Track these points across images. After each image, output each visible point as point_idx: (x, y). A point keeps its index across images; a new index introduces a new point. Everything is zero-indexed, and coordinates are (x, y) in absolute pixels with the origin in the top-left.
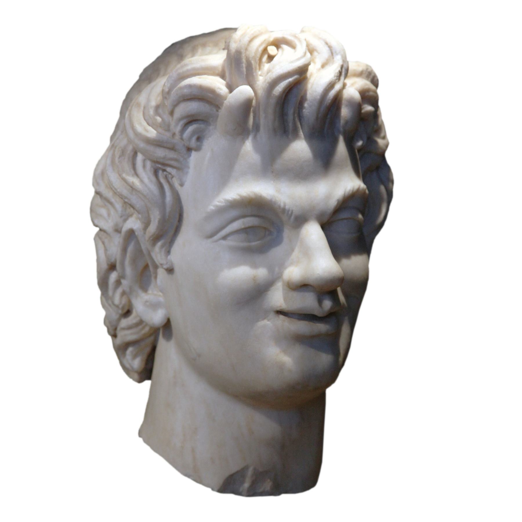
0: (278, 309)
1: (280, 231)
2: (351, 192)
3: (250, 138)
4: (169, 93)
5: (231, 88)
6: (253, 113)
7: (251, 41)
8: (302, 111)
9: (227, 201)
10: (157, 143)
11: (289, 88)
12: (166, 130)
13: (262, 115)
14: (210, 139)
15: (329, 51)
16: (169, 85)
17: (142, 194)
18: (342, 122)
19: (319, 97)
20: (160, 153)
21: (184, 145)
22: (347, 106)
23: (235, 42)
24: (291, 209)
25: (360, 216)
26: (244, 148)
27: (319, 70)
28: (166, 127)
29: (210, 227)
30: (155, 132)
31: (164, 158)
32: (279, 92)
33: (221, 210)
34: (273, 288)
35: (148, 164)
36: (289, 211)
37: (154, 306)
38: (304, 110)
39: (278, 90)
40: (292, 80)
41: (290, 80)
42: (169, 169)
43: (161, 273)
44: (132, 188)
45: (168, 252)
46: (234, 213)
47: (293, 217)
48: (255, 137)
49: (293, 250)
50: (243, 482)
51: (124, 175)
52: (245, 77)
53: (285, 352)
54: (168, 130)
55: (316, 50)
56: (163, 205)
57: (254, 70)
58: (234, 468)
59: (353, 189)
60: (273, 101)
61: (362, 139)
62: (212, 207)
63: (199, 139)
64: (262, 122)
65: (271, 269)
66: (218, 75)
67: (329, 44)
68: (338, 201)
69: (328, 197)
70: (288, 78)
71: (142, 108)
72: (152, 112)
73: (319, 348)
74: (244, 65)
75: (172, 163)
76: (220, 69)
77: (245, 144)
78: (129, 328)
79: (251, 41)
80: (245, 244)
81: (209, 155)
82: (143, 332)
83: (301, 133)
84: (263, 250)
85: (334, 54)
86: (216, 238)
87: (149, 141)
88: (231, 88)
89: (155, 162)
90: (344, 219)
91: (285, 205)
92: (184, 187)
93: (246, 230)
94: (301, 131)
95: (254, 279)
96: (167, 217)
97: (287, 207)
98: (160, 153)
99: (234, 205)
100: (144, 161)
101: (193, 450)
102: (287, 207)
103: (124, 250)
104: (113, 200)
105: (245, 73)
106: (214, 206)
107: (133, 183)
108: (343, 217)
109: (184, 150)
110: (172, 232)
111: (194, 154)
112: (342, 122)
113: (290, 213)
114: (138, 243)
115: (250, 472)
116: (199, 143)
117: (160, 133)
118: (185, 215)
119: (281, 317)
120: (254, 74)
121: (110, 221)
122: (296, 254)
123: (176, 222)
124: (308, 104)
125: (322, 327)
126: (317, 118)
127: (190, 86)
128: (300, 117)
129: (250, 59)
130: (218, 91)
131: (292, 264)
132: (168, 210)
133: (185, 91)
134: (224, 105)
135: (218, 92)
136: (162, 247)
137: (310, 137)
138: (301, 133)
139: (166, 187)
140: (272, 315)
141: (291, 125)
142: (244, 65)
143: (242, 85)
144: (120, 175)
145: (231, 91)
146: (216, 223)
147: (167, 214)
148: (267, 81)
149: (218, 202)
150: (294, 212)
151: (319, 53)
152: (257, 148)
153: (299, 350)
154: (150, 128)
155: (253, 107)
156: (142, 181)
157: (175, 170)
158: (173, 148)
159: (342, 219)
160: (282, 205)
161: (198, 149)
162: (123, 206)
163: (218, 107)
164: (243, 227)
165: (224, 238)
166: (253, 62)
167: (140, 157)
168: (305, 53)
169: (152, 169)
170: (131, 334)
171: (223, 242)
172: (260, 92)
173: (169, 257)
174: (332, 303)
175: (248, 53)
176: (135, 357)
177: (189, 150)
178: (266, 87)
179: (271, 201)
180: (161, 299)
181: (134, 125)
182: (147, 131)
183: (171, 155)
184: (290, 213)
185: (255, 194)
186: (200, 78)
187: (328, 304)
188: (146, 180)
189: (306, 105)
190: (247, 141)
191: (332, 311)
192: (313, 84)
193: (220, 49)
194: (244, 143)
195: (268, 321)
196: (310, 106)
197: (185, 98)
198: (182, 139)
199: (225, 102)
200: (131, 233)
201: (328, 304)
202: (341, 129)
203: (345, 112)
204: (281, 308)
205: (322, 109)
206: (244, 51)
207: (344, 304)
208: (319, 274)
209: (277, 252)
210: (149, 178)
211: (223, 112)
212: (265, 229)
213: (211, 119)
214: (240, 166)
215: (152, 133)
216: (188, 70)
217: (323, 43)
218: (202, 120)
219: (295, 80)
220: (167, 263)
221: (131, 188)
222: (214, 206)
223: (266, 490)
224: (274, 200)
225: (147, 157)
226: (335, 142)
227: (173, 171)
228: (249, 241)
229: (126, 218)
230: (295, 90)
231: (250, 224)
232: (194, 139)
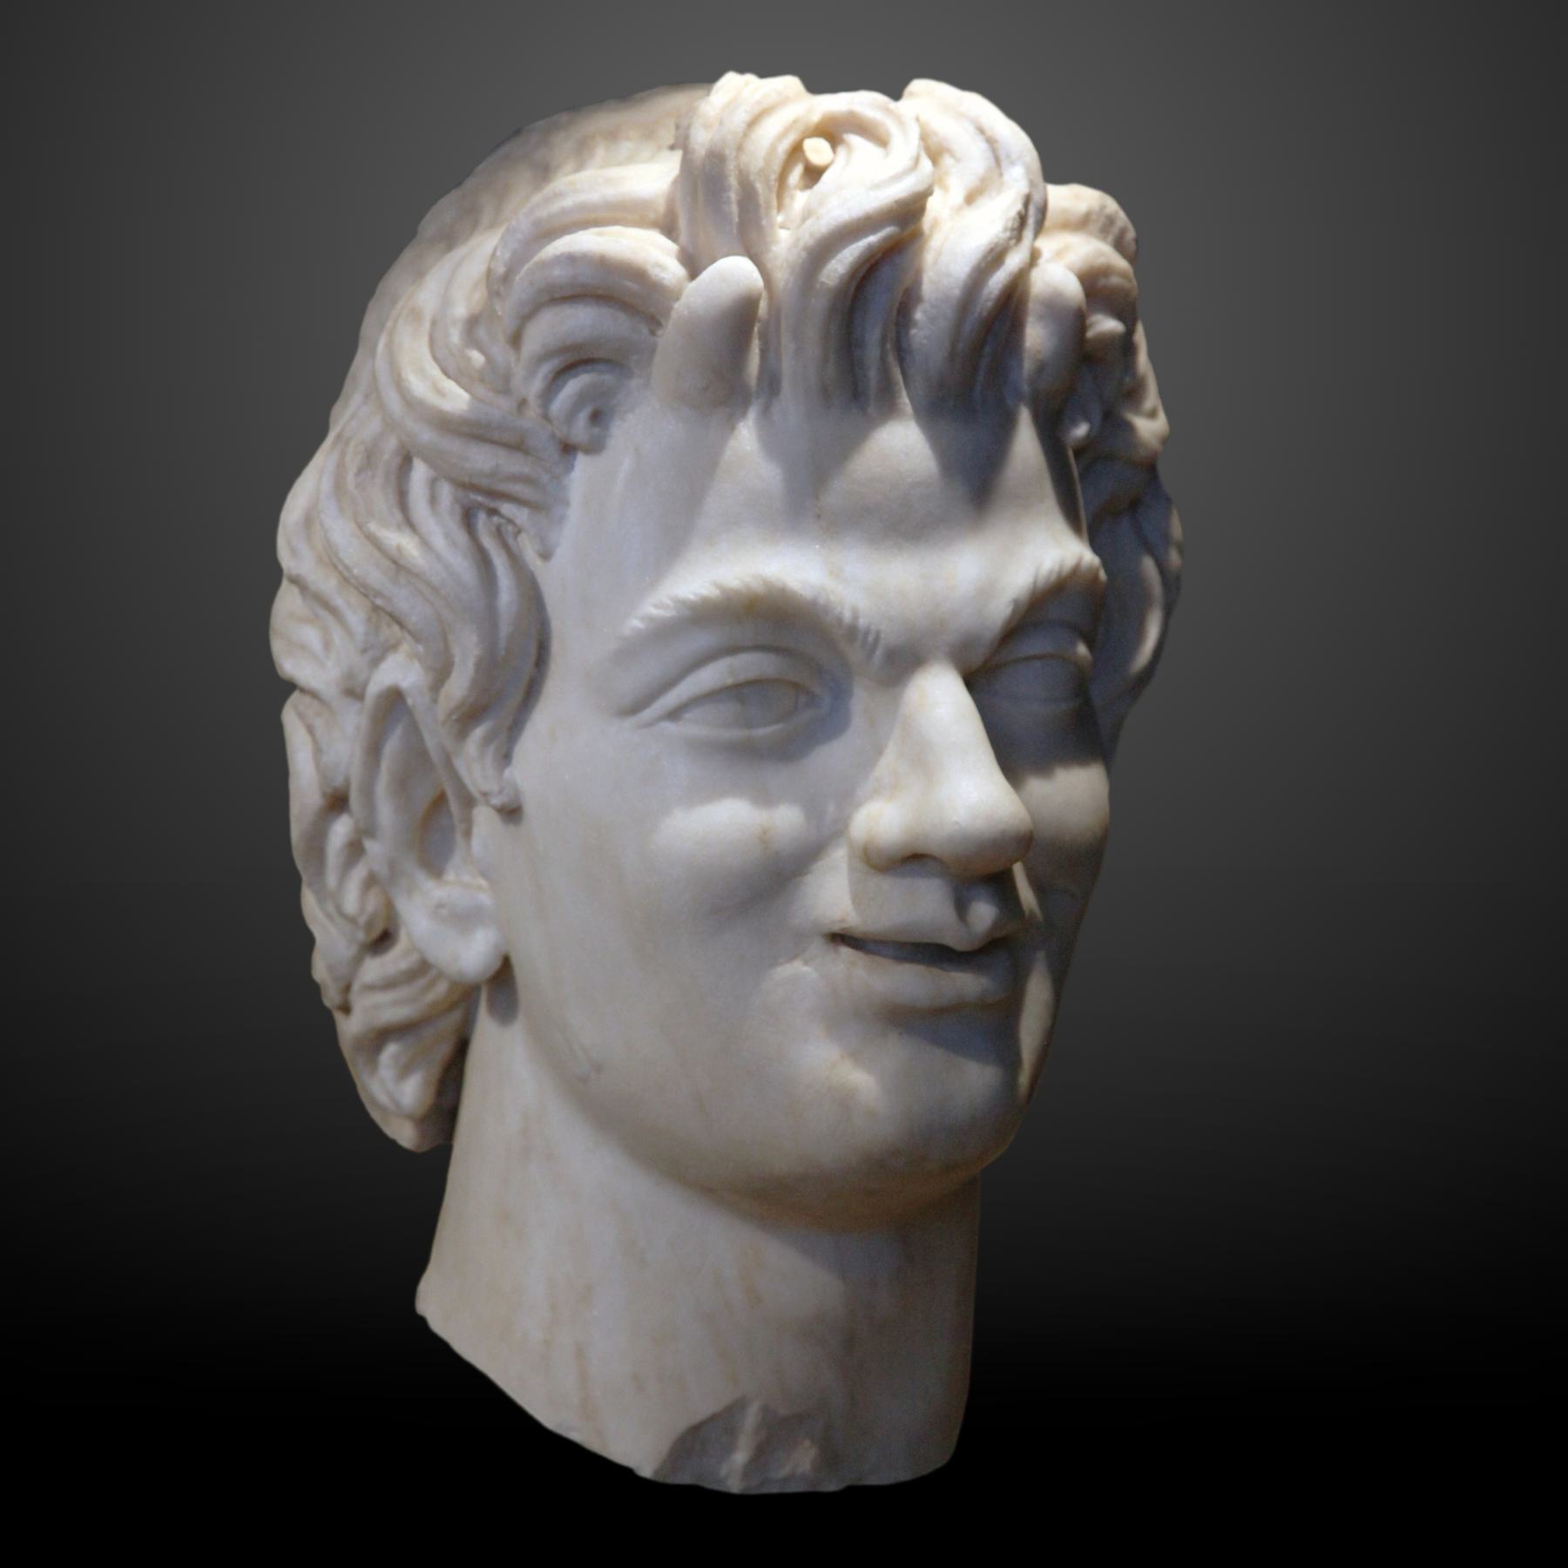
0: (836, 928)
1: (840, 694)
2: (1053, 577)
3: (752, 414)
4: (506, 278)
5: (693, 265)
6: (760, 339)
7: (753, 123)
8: (907, 333)
9: (683, 603)
10: (472, 430)
11: (868, 265)
12: (498, 392)
13: (787, 346)
14: (630, 416)
15: (989, 154)
16: (507, 256)
17: (428, 583)
18: (1028, 366)
19: (957, 292)
20: (481, 460)
21: (553, 436)
22: (1041, 317)
23: (707, 126)
24: (873, 627)
25: (1082, 649)
26: (732, 443)
27: (958, 210)
28: (498, 380)
29: (631, 682)
30: (465, 396)
31: (493, 474)
32: (837, 275)
33: (663, 632)
34: (820, 866)
35: (446, 492)
36: (867, 633)
37: (464, 919)
38: (913, 331)
39: (836, 270)
40: (879, 241)
41: (873, 239)
42: (507, 509)
43: (485, 820)
44: (398, 565)
45: (506, 758)
46: (703, 640)
47: (879, 653)
48: (766, 412)
49: (879, 751)
50: (729, 1448)
51: (373, 526)
52: (735, 231)
53: (856, 1056)
54: (505, 390)
55: (949, 151)
56: (489, 617)
57: (762, 211)
58: (703, 1407)
59: (1061, 566)
60: (819, 304)
61: (1088, 419)
62: (637, 623)
63: (597, 417)
64: (787, 365)
65: (813, 809)
66: (654, 225)
67: (989, 133)
68: (1016, 602)
69: (986, 592)
70: (866, 235)
71: (427, 325)
72: (455, 336)
73: (958, 1047)
74: (733, 196)
75: (517, 489)
76: (661, 207)
77: (736, 432)
78: (389, 984)
79: (753, 123)
80: (737, 734)
81: (627, 465)
82: (431, 997)
83: (905, 400)
84: (789, 750)
85: (1004, 163)
86: (648, 714)
87: (447, 424)
88: (693, 265)
89: (466, 486)
90: (1035, 658)
91: (855, 617)
92: (554, 561)
93: (738, 692)
94: (904, 393)
95: (764, 838)
96: (503, 653)
97: (862, 622)
98: (481, 460)
99: (702, 615)
100: (433, 484)
101: (580, 1353)
102: (862, 622)
103: (374, 750)
104: (338, 601)
105: (737, 220)
106: (642, 619)
107: (399, 549)
108: (1031, 652)
109: (552, 452)
110: (516, 698)
111: (582, 462)
112: (1028, 366)
113: (871, 639)
115: (751, 1418)
116: (596, 430)
117: (481, 401)
118: (555, 646)
119: (846, 952)
120: (764, 222)
121: (330, 664)
122: (889, 762)
123: (528, 668)
124: (925, 312)
125: (966, 984)
126: (952, 355)
127: (571, 259)
128: (902, 351)
129: (752, 178)
130: (655, 273)
131: (876, 792)
132: (505, 630)
133: (557, 272)
134: (674, 315)
135: (654, 277)
136: (487, 740)
137: (932, 413)
138: (905, 400)
139: (500, 562)
140: (817, 946)
141: (873, 374)
142: (733, 196)
143: (727, 255)
144: (360, 526)
145: (694, 273)
146: (649, 669)
147: (502, 644)
148: (801, 244)
149: (656, 606)
150: (882, 636)
151: (958, 160)
152: (771, 444)
153: (897, 1051)
154: (450, 385)
155: (759, 321)
156: (426, 544)
157: (526, 511)
158: (518, 446)
159: (1028, 659)
160: (847, 616)
161: (595, 447)
162: (369, 620)
163: (654, 322)
164: (730, 681)
165: (674, 714)
166: (759, 186)
167: (420, 473)
168: (917, 161)
169: (458, 509)
170: (395, 1003)
171: (670, 727)
173: (507, 772)
174: (998, 911)
175: (744, 158)
176: (404, 1071)
177: (568, 449)
178: (800, 261)
179: (813, 603)
180: (485, 899)
181: (403, 376)
182: (440, 392)
183: (514, 464)
184: (871, 639)
185: (767, 583)
186: (600, 234)
187: (984, 913)
188: (439, 542)
189: (919, 315)
190: (742, 424)
191: (998, 935)
192: (939, 253)
193: (659, 148)
194: (733, 428)
195: (806, 963)
196: (932, 319)
197: (556, 295)
198: (546, 417)
199: (676, 306)
200: (394, 700)
201: (984, 913)
202: (1026, 388)
203: (1036, 336)
204: (845, 925)
205: (967, 328)
206: (734, 154)
207: (1032, 913)
208: (957, 823)
209: (831, 757)
210: (447, 535)
211: (668, 336)
212: (796, 686)
213: (635, 357)
214: (721, 497)
215: (456, 399)
216: (564, 212)
217: (972, 129)
218: (607, 361)
219: (885, 239)
220: (501, 791)
221: (393, 566)
222: (642, 619)
223: (800, 1470)
224: (822, 601)
225: (443, 471)
226: (1006, 426)
227: (520, 515)
228: (749, 725)
229: (377, 654)
230: (885, 272)
231: (752, 674)
232: (583, 417)
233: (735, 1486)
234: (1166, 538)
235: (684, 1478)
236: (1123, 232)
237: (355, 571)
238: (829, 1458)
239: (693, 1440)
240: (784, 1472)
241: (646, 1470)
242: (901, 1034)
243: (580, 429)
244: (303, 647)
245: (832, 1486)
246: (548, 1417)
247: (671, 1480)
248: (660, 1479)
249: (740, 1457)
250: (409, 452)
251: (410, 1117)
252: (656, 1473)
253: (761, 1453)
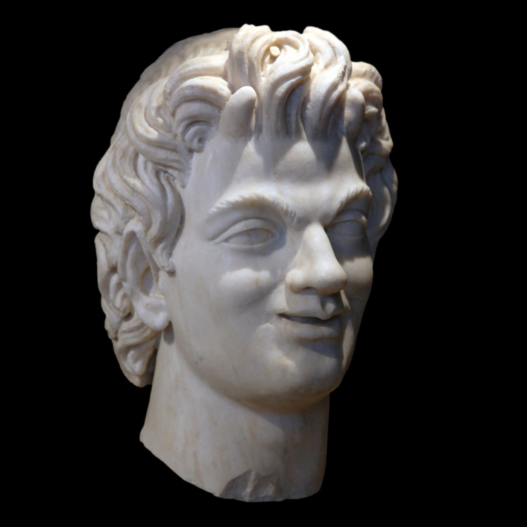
0: (281, 312)
1: (282, 233)
2: (354, 194)
3: (253, 139)
4: (170, 94)
5: (233, 89)
6: (255, 114)
7: (253, 41)
8: (305, 112)
9: (230, 203)
10: (159, 145)
11: (292, 89)
12: (167, 132)
13: (265, 116)
14: (212, 140)
15: (332, 52)
16: (170, 86)
17: (144, 196)
18: (345, 123)
19: (322, 98)
20: (162, 154)
21: (186, 147)
22: (350, 107)
23: (237, 43)
24: (293, 211)
25: (364, 218)
26: (246, 149)
27: (322, 70)
28: (168, 128)
29: (212, 229)
30: (156, 133)
31: (166, 159)
32: (281, 92)
33: (223, 212)
34: (276, 291)
35: (150, 165)
36: (291, 213)
37: (156, 309)
38: (307, 111)
39: (281, 91)
40: (295, 81)
41: (293, 80)
42: (170, 171)
43: (163, 276)
44: (134, 190)
45: (170, 255)
46: (236, 215)
47: (295, 219)
48: (257, 138)
49: (295, 253)
50: (245, 487)
51: (125, 177)
52: (247, 78)
53: (288, 355)
55: (319, 51)
56: (164, 207)
57: (256, 71)
58: (236, 473)
59: (357, 190)
60: (275, 102)
61: (366, 141)
62: (214, 209)
63: (201, 140)
64: (265, 123)
65: (273, 272)
66: (220, 76)
67: (332, 45)
68: (341, 202)
69: (331, 199)
70: (291, 79)
71: (144, 109)
72: (153, 113)
73: (322, 352)
74: (246, 66)
75: (174, 164)
76: (222, 70)
77: (247, 145)
78: (131, 331)
79: (253, 41)
80: (248, 247)
81: (211, 156)
82: (145, 335)
83: (304, 135)
84: (265, 252)
85: (337, 55)
86: (218, 240)
87: (150, 143)
88: (233, 89)
89: (157, 163)
90: (348, 221)
91: (288, 207)
92: (186, 188)
93: (248, 232)
94: (304, 132)
95: (257, 282)
96: (169, 219)
97: (290, 209)
98: (162, 154)
99: (236, 207)
100: (145, 163)
101: (195, 455)
102: (290, 209)
103: (126, 252)
104: (114, 202)
105: (248, 74)
106: (216, 208)
107: (134, 184)
108: (347, 219)
109: (186, 152)
110: (173, 235)
111: (196, 155)
112: (345, 123)
113: (293, 215)
115: (252, 477)
116: (200, 145)
117: (162, 135)
118: (187, 217)
119: (284, 320)
120: (257, 75)
121: (111, 223)
122: (299, 256)
123: (177, 225)
124: (311, 105)
125: (325, 331)
126: (320, 119)
127: (192, 87)
128: (303, 118)
129: (253, 60)
130: (220, 92)
131: (294, 266)
132: (170, 212)
133: (187, 91)
134: (226, 106)
135: (220, 93)
136: (164, 249)
137: (313, 139)
138: (304, 135)
139: (168, 189)
140: (275, 318)
141: (293, 126)
142: (246, 66)
143: (244, 86)
144: (121, 177)
145: (233, 92)
146: (218, 225)
147: (169, 216)
148: (269, 82)
149: (220, 204)
150: (297, 214)
151: (322, 54)
152: (259, 149)
153: (301, 353)
154: (151, 130)
155: (255, 108)
156: (143, 183)
157: (177, 172)
158: (174, 150)
159: (346, 221)
160: (285, 207)
161: (200, 150)
162: (124, 208)
163: (220, 108)
164: (245, 229)
165: (227, 240)
166: (255, 63)
167: (141, 159)
168: (308, 54)
169: (154, 171)
170: (133, 337)
171: (225, 244)
172: (263, 93)
173: (170, 260)
174: (335, 306)
175: (250, 53)
176: (136, 360)
177: (191, 151)
178: (269, 88)
179: (273, 203)
180: (163, 302)
181: (136, 126)
182: (148, 132)
183: (173, 156)
184: (293, 215)
185: (258, 196)
186: (202, 79)
187: (331, 307)
188: (148, 182)
189: (309, 106)
190: (249, 142)
192: (316, 85)
193: (222, 50)
194: (246, 144)
195: (271, 324)
196: (313, 107)
197: (187, 99)
198: (183, 140)
199: (227, 103)
200: (132, 235)
201: (331, 307)
202: (345, 130)
203: (348, 113)
204: (284, 311)
205: (325, 110)
206: (247, 52)
207: (347, 307)
208: (322, 277)
209: (279, 254)
210: (150, 180)
211: (225, 113)
212: (268, 231)
213: (213, 120)
214: (242, 167)
215: (153, 134)
216: (190, 71)
217: (327, 43)
218: (204, 121)
219: (298, 80)
220: (168, 266)
221: (132, 190)
222: (216, 208)
223: (269, 494)
224: (276, 202)
225: (149, 158)
227: (175, 173)
228: (252, 244)
229: (127, 220)
230: (298, 91)
231: (253, 227)
232: (196, 140)
233: (247, 499)
234: (392, 181)
235: (230, 497)
236: (377, 78)
237: (119, 192)
238: (279, 490)
239: (233, 484)
240: (263, 495)
241: (217, 494)
242: (303, 347)
243: (195, 144)
244: (102, 218)
245: (280, 499)
246: (184, 476)
247: (225, 497)
248: (222, 497)
249: (249, 490)
250: (137, 152)
251: (138, 375)
252: (221, 495)
253: (256, 488)
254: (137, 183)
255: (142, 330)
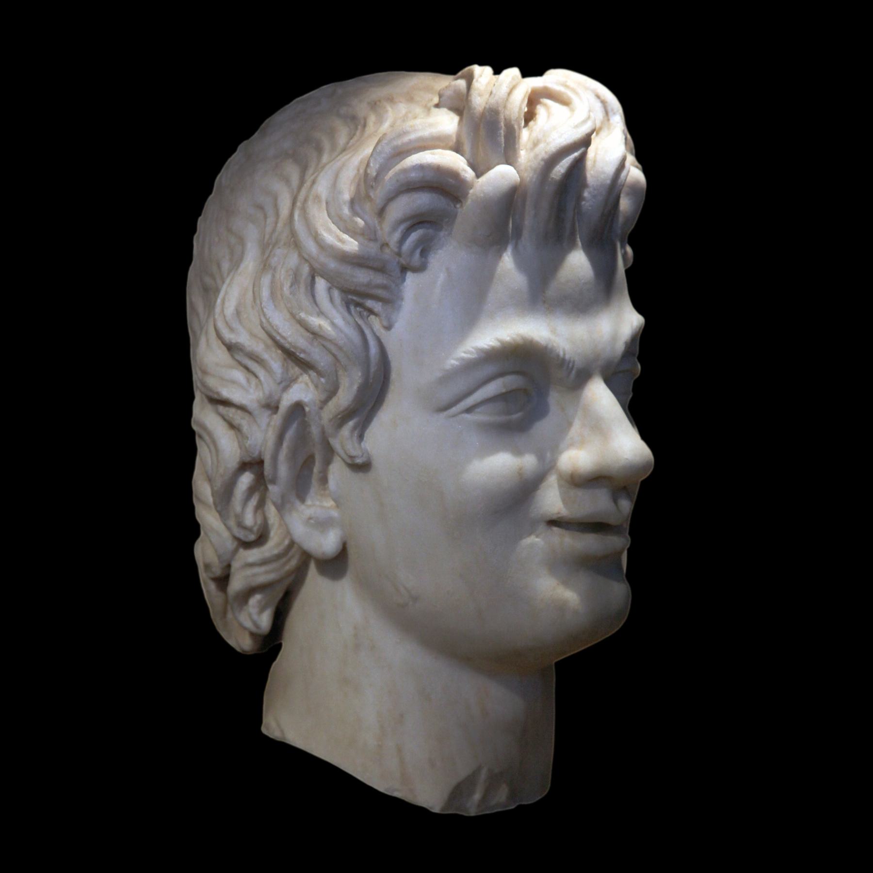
0: (548, 519)
7: (510, 93)
9: (481, 351)
12: (370, 240)
14: (440, 251)
16: (378, 166)
17: (336, 345)
19: (608, 182)
20: (362, 277)
21: (398, 263)
22: (628, 194)
23: (480, 95)
26: (501, 264)
28: (368, 235)
29: (446, 394)
30: (356, 243)
31: (368, 285)
32: (560, 174)
33: (469, 366)
34: (544, 484)
35: (336, 293)
36: (570, 362)
37: (322, 524)
39: (560, 171)
43: (337, 472)
44: (315, 335)
45: (361, 437)
46: (490, 369)
47: (574, 372)
49: (570, 424)
52: (502, 151)
53: (565, 583)
54: (375, 240)
58: (463, 772)
60: (550, 189)
63: (424, 253)
65: (541, 457)
67: (603, 98)
68: (626, 343)
69: (614, 338)
70: (573, 152)
71: (324, 204)
72: (346, 211)
74: (502, 132)
75: (380, 292)
76: (454, 139)
77: (503, 258)
78: (264, 562)
79: (510, 93)
81: (442, 277)
82: (287, 568)
85: (610, 114)
86: (454, 410)
87: (345, 258)
89: (346, 291)
91: (564, 354)
92: (393, 330)
95: (520, 472)
97: (567, 357)
98: (362, 277)
100: (329, 290)
101: (399, 750)
103: (280, 438)
104: (266, 356)
105: (504, 145)
106: (457, 359)
107: (320, 326)
109: (397, 272)
111: (410, 277)
112: (621, 219)
113: (571, 365)
114: (304, 427)
116: (423, 259)
118: (394, 376)
121: (252, 391)
122: (576, 429)
124: (589, 193)
127: (421, 167)
129: (513, 122)
131: (571, 445)
133: (413, 175)
136: (354, 428)
137: (588, 249)
139: (367, 332)
140: (542, 527)
141: (568, 225)
142: (502, 132)
143: (498, 164)
144: (293, 316)
145: (479, 175)
146: (461, 385)
147: (372, 376)
148: (540, 157)
149: (465, 352)
150: (576, 363)
152: (521, 264)
154: (346, 237)
156: (333, 324)
161: (421, 268)
162: (283, 365)
164: (504, 390)
165: (469, 410)
167: (321, 284)
170: (267, 572)
171: (468, 416)
173: (362, 444)
175: (507, 113)
176: (262, 610)
177: (404, 269)
178: (540, 166)
179: (546, 348)
180: (335, 514)
181: (319, 232)
183: (379, 279)
184: (571, 365)
185: (524, 339)
186: (433, 154)
188: (339, 321)
189: (586, 194)
190: (505, 254)
192: (595, 162)
193: (428, 110)
194: (500, 256)
195: (537, 537)
197: (411, 187)
198: (399, 254)
199: (471, 191)
200: (298, 408)
202: (619, 232)
203: (625, 204)
204: (559, 516)
208: (627, 459)
209: (543, 427)
210: (344, 319)
211: (467, 210)
214: (497, 292)
215: (351, 245)
216: (411, 141)
220: (362, 456)
221: (311, 336)
222: (457, 359)
224: (550, 346)
225: (333, 281)
227: (377, 306)
229: (287, 383)
232: (418, 252)
233: (473, 812)
237: (290, 339)
238: (512, 795)
239: (459, 791)
241: (436, 809)
244: (233, 382)
249: (477, 796)
251: (253, 635)
254: (316, 321)
255: (284, 560)
